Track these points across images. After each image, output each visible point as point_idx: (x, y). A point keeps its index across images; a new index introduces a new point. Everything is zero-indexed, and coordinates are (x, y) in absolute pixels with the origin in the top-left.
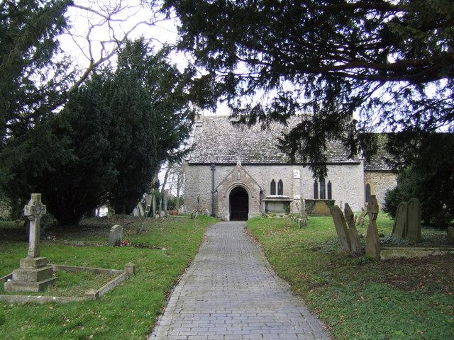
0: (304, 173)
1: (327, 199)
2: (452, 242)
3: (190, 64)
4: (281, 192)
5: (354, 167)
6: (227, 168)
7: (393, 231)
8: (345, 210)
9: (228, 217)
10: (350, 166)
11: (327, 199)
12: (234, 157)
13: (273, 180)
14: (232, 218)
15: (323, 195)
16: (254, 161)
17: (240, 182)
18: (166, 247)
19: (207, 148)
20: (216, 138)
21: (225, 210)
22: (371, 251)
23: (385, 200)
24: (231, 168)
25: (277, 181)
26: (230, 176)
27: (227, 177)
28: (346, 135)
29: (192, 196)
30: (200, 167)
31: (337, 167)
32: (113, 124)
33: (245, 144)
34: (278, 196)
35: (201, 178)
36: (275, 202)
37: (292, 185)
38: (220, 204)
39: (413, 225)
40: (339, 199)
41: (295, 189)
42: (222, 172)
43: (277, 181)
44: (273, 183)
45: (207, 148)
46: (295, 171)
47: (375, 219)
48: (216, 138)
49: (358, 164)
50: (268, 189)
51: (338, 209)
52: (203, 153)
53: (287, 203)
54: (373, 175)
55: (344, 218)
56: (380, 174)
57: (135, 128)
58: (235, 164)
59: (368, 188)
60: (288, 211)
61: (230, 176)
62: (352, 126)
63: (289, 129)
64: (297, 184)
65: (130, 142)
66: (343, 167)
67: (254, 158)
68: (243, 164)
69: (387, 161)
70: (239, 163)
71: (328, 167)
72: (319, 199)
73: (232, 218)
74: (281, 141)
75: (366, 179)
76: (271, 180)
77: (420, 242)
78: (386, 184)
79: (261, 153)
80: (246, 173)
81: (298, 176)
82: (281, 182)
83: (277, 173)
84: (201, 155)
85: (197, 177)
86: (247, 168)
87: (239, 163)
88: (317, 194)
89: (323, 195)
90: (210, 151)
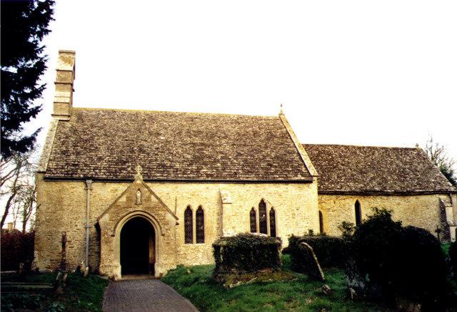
3: (41, 40)
5: (305, 186)
10: (301, 185)
13: (253, 209)
15: (263, 224)
17: (139, 210)
18: (164, 136)
24: (122, 187)
25: (195, 209)
26: (124, 199)
27: (116, 201)
29: (50, 234)
33: (141, 151)
43: (195, 209)
44: (188, 211)
45: (78, 153)
48: (92, 138)
49: (311, 182)
54: (325, 196)
56: (334, 197)
66: (290, 186)
80: (152, 193)
82: (200, 212)
85: (60, 201)
86: (149, 184)
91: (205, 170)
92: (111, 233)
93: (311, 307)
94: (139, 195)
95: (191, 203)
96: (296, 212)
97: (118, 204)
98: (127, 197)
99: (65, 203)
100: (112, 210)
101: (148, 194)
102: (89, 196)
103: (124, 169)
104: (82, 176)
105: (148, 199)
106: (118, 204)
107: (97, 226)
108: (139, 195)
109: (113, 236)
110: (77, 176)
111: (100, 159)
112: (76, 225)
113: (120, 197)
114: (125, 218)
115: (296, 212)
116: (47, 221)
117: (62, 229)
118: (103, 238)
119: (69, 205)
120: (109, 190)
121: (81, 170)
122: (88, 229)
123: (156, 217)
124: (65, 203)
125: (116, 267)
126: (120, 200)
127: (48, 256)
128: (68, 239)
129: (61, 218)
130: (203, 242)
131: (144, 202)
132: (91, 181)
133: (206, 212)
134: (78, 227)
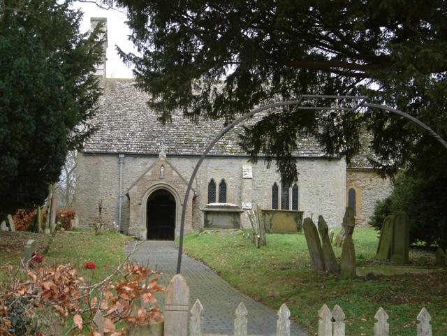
0: (258, 171)
1: (291, 209)
2: (441, 263)
4: (223, 198)
6: (141, 161)
7: (378, 252)
8: (319, 223)
9: (144, 234)
11: (291, 209)
12: (154, 144)
13: (275, 184)
14: (150, 237)
15: (285, 205)
16: (185, 151)
17: (163, 183)
19: (112, 129)
20: (125, 113)
21: (139, 225)
22: (346, 265)
23: (375, 214)
24: (150, 162)
25: (218, 182)
26: (149, 173)
27: (143, 176)
28: (321, 131)
30: (102, 159)
31: (307, 163)
32: (13, 105)
34: (219, 204)
35: (102, 174)
36: (218, 213)
37: (241, 188)
38: (132, 215)
39: (400, 243)
40: (309, 207)
41: (244, 195)
42: (138, 166)
43: (218, 182)
44: (212, 184)
45: (112, 129)
46: (245, 167)
47: (351, 233)
48: (125, 113)
50: (204, 193)
51: (309, 221)
52: (105, 137)
53: (235, 213)
54: (359, 175)
55: (316, 232)
57: (40, 110)
58: (156, 156)
59: (352, 195)
60: (237, 225)
61: (149, 173)
62: (329, 120)
63: (253, 122)
64: (248, 186)
65: (35, 128)
67: (184, 147)
68: (168, 156)
69: (372, 162)
70: (163, 154)
71: (299, 166)
72: (280, 209)
73: (150, 237)
74: (241, 137)
75: (348, 182)
76: (209, 181)
77: (409, 263)
78: (378, 190)
79: (194, 138)
80: (173, 168)
81: (250, 175)
82: (223, 185)
83: (214, 171)
84: (103, 139)
86: (174, 161)
87: (163, 154)
88: (293, 198)
89: (285, 205)
90: (116, 134)
91: (230, 146)
92: (138, 202)
93: (444, 250)
94: (162, 170)
95: (214, 177)
96: (321, 189)
97: (144, 177)
98: (152, 172)
99: (101, 175)
100: (140, 182)
101: (170, 169)
102: (121, 169)
103: (154, 144)
104: (115, 151)
105: (171, 174)
106: (144, 177)
107: (128, 195)
108: (162, 170)
109: (140, 204)
110: (112, 151)
111: (133, 134)
112: (111, 195)
113: (147, 172)
114: (146, 194)
115: (321, 189)
116: (87, 190)
117: (99, 198)
118: (131, 206)
119: (105, 177)
120: (139, 163)
121: (115, 145)
122: (121, 198)
123: (176, 189)
124: (101, 175)
125: (143, 230)
126: (147, 174)
127: (87, 220)
128: (103, 206)
129: (97, 188)
130: (170, 236)
131: (167, 177)
132: (123, 156)
133: (229, 186)
134: (112, 196)
